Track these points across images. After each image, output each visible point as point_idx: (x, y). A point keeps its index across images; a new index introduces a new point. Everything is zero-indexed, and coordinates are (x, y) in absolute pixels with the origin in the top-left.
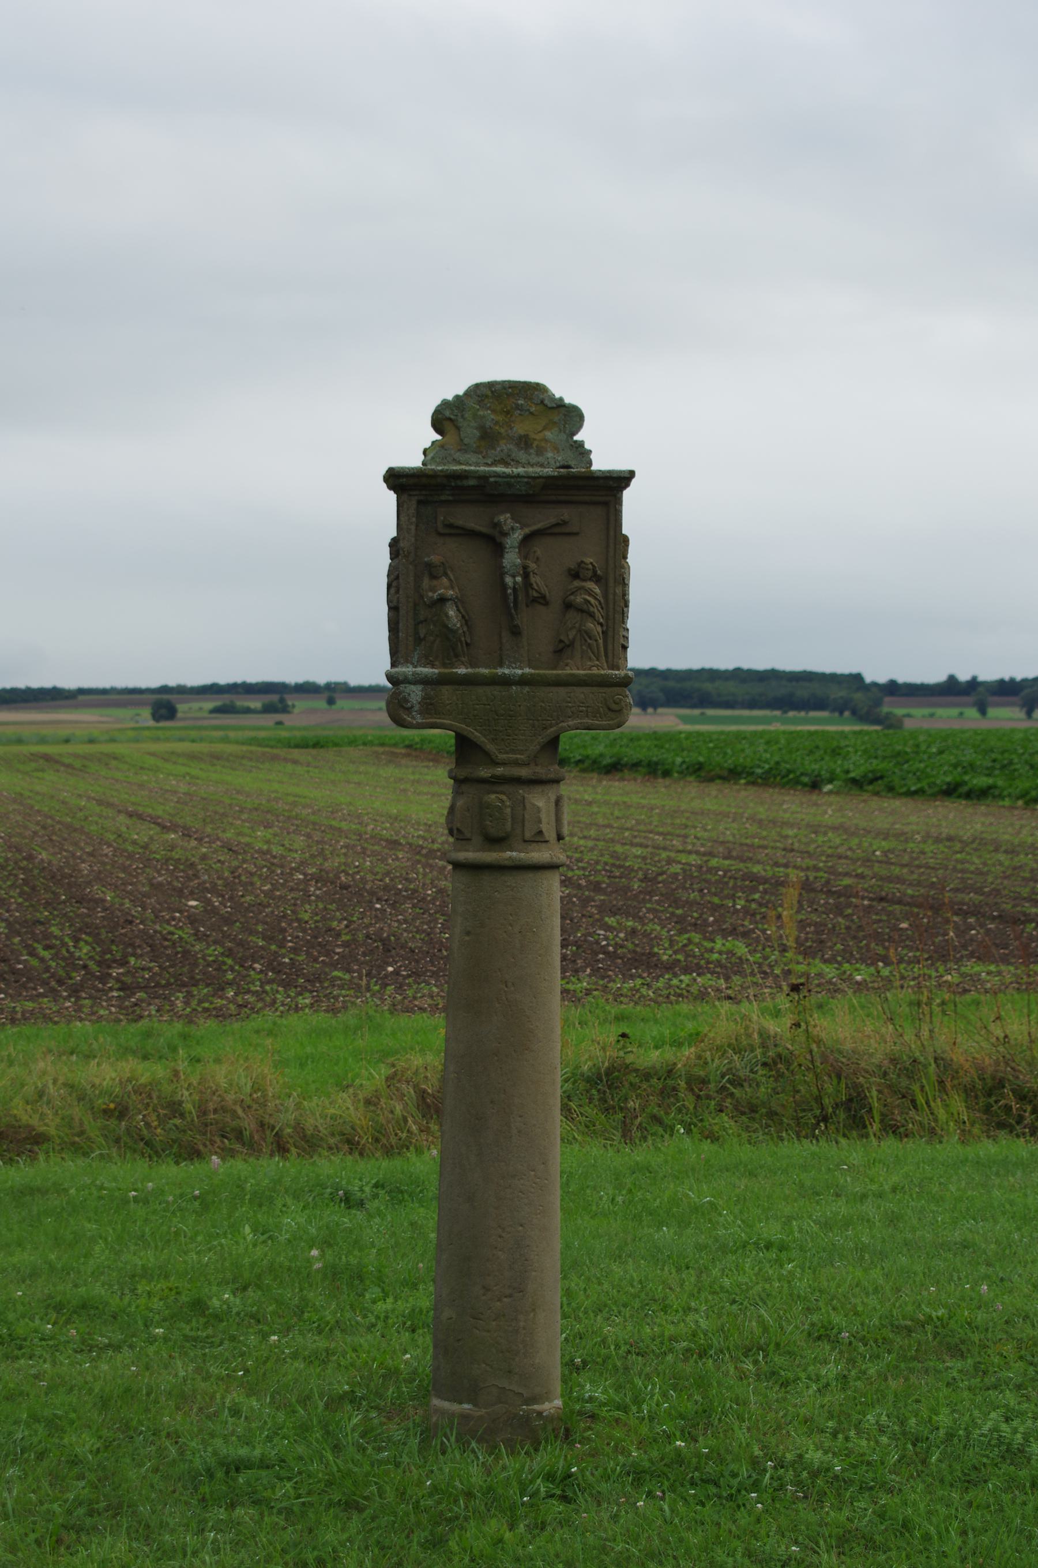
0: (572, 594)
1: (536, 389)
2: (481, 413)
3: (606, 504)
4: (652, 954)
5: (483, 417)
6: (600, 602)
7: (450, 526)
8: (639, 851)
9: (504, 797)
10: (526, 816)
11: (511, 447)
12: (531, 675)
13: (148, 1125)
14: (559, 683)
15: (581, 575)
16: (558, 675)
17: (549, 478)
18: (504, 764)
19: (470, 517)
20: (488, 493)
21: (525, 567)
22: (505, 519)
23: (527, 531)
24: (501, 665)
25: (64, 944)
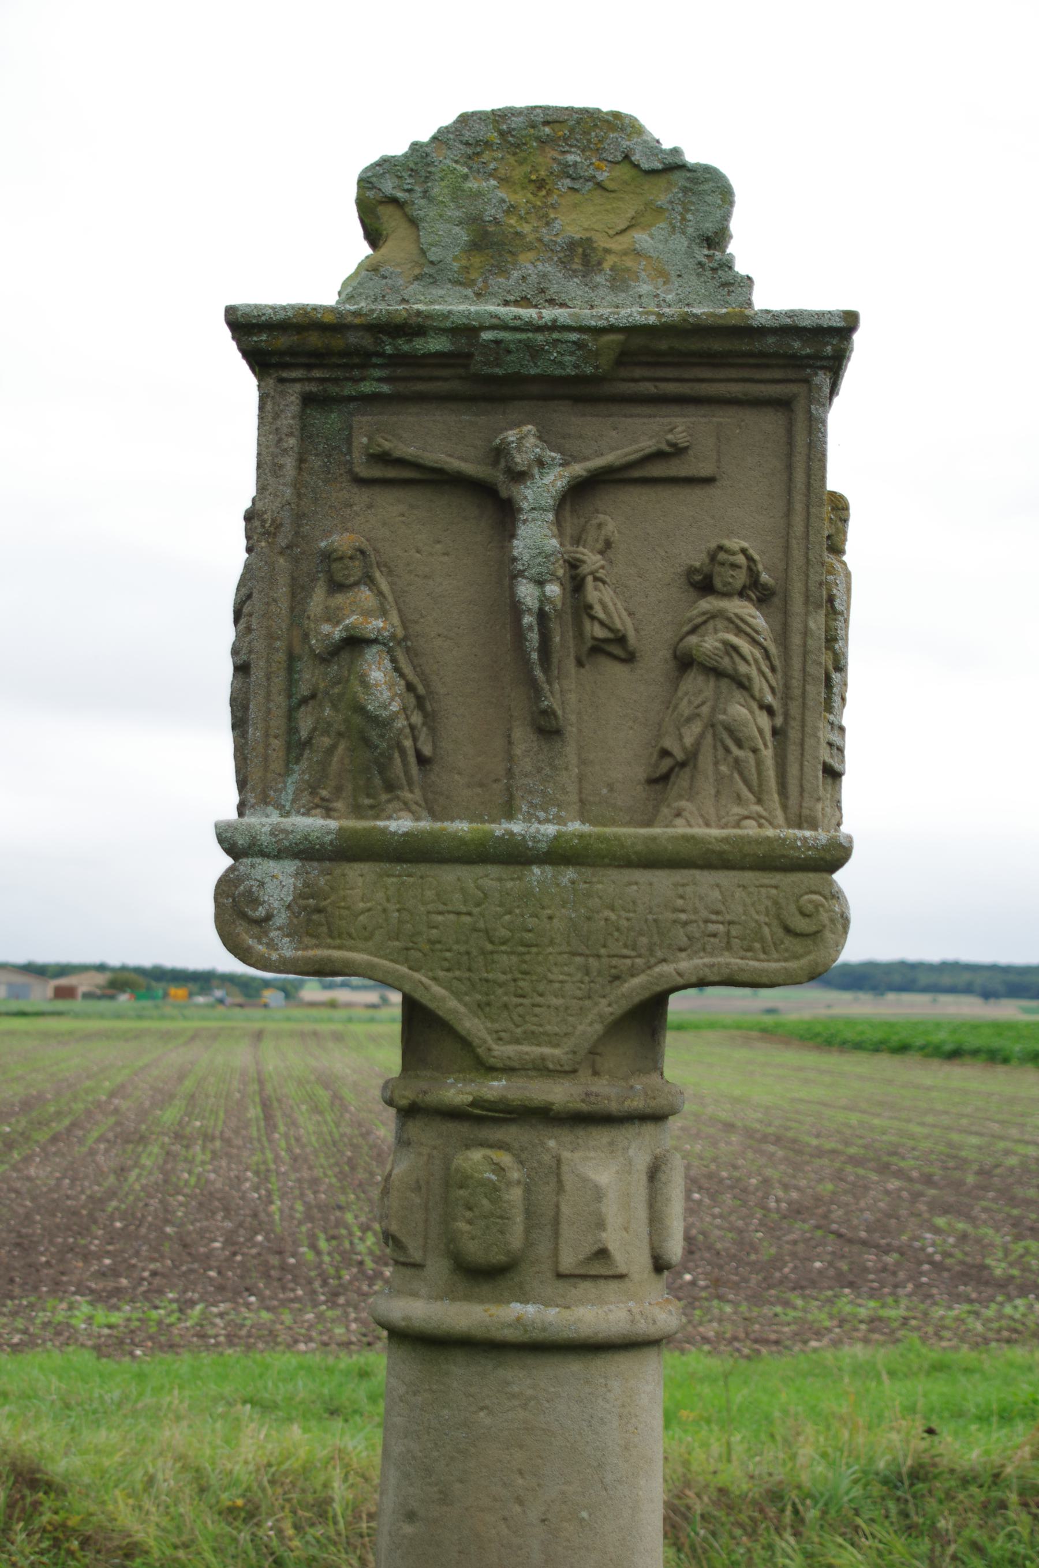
0: (694, 630)
1: (618, 124)
2: (472, 184)
3: (784, 404)
4: (984, 1267)
5: (479, 194)
6: (767, 655)
7: (384, 458)
8: (974, 1140)
9: (505, 1159)
10: (565, 1209)
11: (548, 268)
12: (581, 836)
13: (280, 1532)
14: (653, 860)
15: (718, 583)
16: (654, 839)
17: (632, 330)
18: (508, 1070)
19: (436, 438)
20: (478, 374)
21: (573, 565)
22: (524, 440)
23: (579, 469)
24: (510, 814)
25: (351, 1234)
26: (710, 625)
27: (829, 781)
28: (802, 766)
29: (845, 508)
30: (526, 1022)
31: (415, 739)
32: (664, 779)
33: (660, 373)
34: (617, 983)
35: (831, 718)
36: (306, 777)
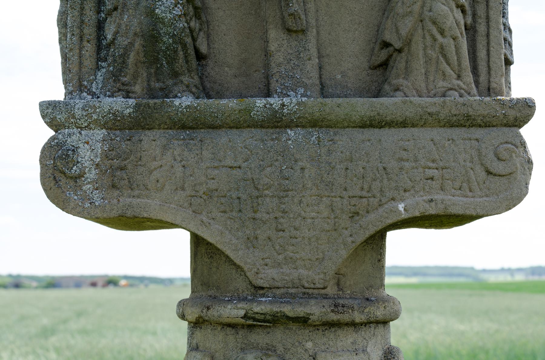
28: (488, 51)
30: (285, 250)
31: (194, 40)
32: (384, 65)
34: (357, 218)
36: (111, 68)
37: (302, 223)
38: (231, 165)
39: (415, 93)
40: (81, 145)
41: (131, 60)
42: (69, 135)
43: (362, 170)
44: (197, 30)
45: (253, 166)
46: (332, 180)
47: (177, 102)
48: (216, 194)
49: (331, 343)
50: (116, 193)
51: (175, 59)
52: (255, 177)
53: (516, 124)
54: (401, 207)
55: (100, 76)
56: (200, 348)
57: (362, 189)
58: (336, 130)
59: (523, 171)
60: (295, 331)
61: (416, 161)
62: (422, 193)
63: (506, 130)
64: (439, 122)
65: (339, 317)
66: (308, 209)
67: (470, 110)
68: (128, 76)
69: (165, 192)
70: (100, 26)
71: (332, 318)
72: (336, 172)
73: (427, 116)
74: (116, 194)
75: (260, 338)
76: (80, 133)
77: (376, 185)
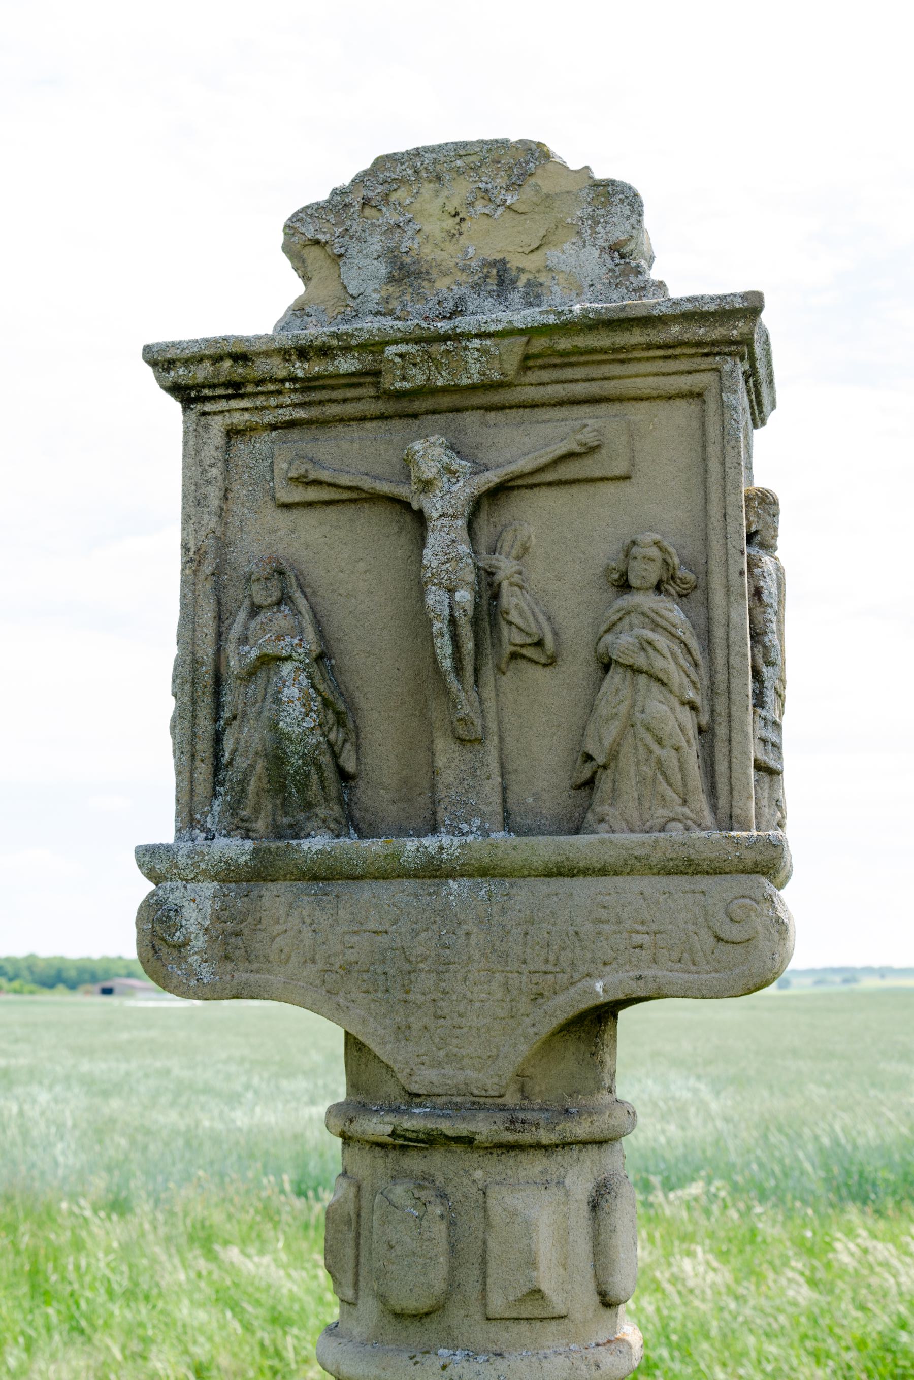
10: (492, 1245)
15: (634, 581)
22: (429, 451)
26: (626, 621)
27: (766, 778)
29: (775, 503)
31: (335, 756)
33: (569, 373)
34: (540, 1001)
35: (763, 713)
36: (228, 798)
37: (469, 1007)
38: (375, 929)
39: (624, 825)
40: (186, 904)
41: (252, 788)
42: (172, 890)
43: (546, 935)
44: (340, 743)
45: (403, 930)
46: (506, 950)
47: (305, 844)
48: (356, 969)
49: (509, 1172)
50: (230, 966)
51: (306, 786)
52: (405, 945)
53: (758, 869)
54: (599, 986)
55: (217, 805)
56: (349, 1174)
57: (547, 961)
58: (513, 880)
59: (767, 936)
60: (460, 1155)
61: (619, 922)
62: (627, 967)
63: (743, 878)
64: (650, 868)
65: (516, 1138)
66: (476, 989)
67: (692, 851)
68: (248, 810)
69: (291, 966)
70: (218, 739)
71: (506, 1139)
72: (511, 939)
73: (633, 861)
74: (230, 968)
75: (415, 1163)
76: (185, 887)
77: (565, 956)
